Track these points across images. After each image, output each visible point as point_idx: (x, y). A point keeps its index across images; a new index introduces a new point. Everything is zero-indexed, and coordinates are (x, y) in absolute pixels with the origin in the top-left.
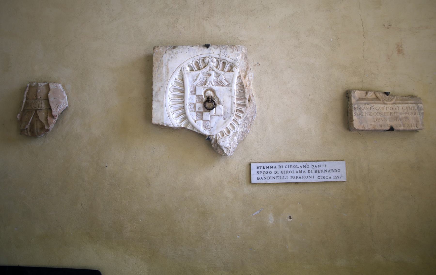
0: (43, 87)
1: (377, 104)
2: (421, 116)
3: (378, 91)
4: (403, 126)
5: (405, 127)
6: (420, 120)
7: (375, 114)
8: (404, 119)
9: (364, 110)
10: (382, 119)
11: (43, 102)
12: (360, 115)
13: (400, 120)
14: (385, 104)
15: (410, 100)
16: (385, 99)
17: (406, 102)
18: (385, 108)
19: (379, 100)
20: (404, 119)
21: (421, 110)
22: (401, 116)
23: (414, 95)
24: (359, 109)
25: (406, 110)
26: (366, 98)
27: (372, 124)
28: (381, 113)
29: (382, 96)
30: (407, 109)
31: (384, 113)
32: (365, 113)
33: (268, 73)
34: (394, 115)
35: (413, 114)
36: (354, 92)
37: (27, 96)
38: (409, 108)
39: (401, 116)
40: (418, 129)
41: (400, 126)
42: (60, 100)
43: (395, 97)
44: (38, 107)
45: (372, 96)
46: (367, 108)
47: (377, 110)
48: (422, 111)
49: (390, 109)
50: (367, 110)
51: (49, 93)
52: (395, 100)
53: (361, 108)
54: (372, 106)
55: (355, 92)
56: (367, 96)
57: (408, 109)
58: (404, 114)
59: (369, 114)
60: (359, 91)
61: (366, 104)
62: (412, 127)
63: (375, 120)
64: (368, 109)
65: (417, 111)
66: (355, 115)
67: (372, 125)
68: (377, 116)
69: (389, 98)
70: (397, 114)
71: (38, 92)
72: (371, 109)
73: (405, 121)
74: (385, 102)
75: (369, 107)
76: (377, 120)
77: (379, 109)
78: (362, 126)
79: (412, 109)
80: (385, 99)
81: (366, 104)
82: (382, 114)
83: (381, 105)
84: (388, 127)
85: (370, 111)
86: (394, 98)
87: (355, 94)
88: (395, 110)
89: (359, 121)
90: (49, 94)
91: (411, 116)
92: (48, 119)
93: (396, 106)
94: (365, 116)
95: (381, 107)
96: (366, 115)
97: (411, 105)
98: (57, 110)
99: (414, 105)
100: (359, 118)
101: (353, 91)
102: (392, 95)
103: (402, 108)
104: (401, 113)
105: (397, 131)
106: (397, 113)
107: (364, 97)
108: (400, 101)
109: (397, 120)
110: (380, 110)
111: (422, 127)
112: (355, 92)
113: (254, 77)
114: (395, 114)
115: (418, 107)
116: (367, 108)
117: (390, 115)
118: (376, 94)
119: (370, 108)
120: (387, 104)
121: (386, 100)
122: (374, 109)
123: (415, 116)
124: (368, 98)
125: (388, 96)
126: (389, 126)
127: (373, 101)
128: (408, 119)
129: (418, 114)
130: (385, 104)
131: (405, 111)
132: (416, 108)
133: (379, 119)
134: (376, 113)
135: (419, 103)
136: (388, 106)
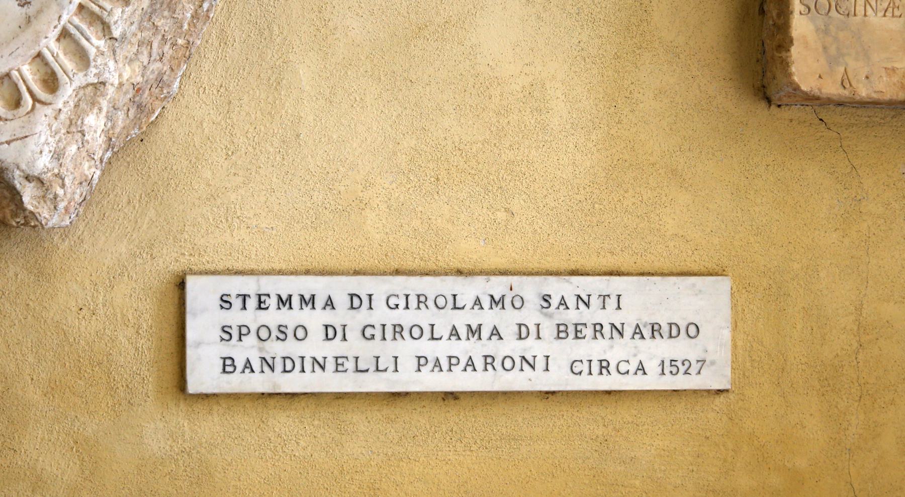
12: (833, 13)
27: (897, 65)
66: (803, 8)
67: (894, 70)
78: (839, 78)
89: (825, 48)
96: (870, 11)
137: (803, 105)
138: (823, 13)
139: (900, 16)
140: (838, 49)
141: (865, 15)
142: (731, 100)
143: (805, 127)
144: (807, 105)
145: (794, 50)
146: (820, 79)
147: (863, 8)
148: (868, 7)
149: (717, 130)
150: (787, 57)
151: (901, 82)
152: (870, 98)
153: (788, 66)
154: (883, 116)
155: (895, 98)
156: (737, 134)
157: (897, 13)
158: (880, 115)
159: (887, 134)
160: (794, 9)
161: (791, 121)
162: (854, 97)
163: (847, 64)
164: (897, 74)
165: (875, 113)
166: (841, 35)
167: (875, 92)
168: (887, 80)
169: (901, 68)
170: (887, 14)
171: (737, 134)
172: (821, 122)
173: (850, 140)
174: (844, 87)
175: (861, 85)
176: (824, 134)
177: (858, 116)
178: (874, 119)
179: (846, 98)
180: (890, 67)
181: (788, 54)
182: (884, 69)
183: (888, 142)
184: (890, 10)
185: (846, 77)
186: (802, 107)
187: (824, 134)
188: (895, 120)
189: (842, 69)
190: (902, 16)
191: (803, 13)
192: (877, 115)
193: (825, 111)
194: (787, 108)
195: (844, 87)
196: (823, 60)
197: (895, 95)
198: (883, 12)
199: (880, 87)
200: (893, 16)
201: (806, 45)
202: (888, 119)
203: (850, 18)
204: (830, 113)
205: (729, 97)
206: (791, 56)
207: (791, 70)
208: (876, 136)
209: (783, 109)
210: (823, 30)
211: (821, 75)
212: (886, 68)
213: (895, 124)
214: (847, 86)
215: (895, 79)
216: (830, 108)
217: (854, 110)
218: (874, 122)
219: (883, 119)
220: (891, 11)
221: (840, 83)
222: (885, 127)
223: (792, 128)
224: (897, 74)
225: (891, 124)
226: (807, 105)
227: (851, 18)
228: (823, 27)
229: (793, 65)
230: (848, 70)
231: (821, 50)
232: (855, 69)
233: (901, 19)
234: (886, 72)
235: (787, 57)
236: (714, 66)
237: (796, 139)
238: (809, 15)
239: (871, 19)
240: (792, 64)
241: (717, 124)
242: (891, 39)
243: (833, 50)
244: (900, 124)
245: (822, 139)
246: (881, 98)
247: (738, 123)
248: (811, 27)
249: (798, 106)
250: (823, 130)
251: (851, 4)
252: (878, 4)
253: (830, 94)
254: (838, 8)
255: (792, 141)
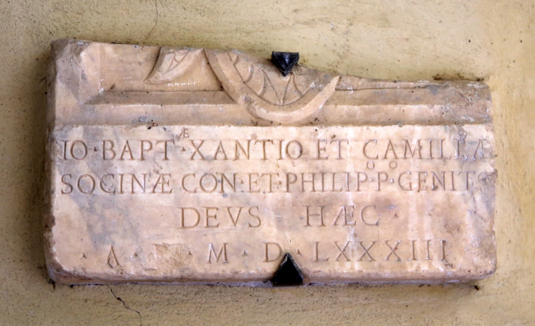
1: (206, 124)
2: (478, 197)
3: (227, 50)
4: (358, 255)
5: (373, 260)
6: (468, 220)
7: (192, 184)
8: (370, 212)
9: (127, 156)
10: (235, 216)
12: (98, 191)
13: (342, 221)
14: (257, 122)
15: (418, 101)
16: (260, 97)
17: (394, 109)
18: (257, 152)
19: (230, 99)
20: (370, 212)
21: (477, 159)
22: (349, 193)
23: (467, 76)
24: (91, 153)
25: (385, 158)
26: (148, 87)
27: (169, 242)
28: (230, 177)
29: (250, 77)
30: (390, 155)
31: (246, 179)
32: (128, 179)
33: (50, 12)
34: (308, 187)
35: (429, 183)
36: (77, 52)
38: (407, 145)
39: (351, 197)
40: (450, 272)
41: (344, 255)
43: (326, 82)
45: (188, 73)
46: (147, 146)
47: (203, 158)
48: (487, 167)
49: (284, 155)
50: (143, 159)
52: (327, 103)
53: (108, 145)
54: (178, 138)
55: (81, 50)
56: (161, 75)
57: (400, 153)
58: (375, 185)
59: (154, 181)
60: (109, 48)
61: (138, 122)
62: (414, 259)
63: (191, 219)
64: (150, 154)
65: (453, 165)
66: (64, 187)
67: (165, 246)
68: (203, 195)
69: (291, 85)
70: (328, 186)
72: (169, 156)
73: (377, 224)
74: (262, 112)
75: (158, 142)
76: (204, 217)
77: (220, 156)
78: (105, 256)
79: (425, 151)
80: (264, 92)
81: (138, 122)
82: (233, 187)
83: (233, 129)
84: (267, 260)
85: (163, 164)
86: (320, 90)
87: (80, 61)
88: (319, 158)
89: (90, 227)
91: (411, 193)
93: (323, 133)
94: (125, 195)
95: (233, 144)
96: (137, 188)
97: (418, 129)
99: (438, 131)
100: (91, 210)
101: (69, 47)
102: (314, 73)
103: (362, 144)
104: (354, 175)
105: (350, 285)
106: (328, 179)
107: (136, 85)
108: (356, 108)
109: (326, 221)
110: (226, 158)
111: (477, 260)
112: (78, 54)
114: (318, 185)
115: (461, 144)
116: (147, 146)
117: (285, 189)
118: (213, 65)
119: (162, 146)
120: (271, 123)
121: (269, 102)
122: (187, 155)
123: (439, 196)
124: (162, 88)
125: (284, 75)
126: (274, 252)
127: (188, 108)
128: (396, 215)
129: (459, 182)
130: (256, 124)
131: (382, 165)
132: (449, 148)
133: (212, 213)
134: (198, 177)
135: (472, 120)
136: (276, 133)
137: (97, 285)
138: (87, 191)
139: (171, 192)
140: (104, 226)
141: (133, 192)
142: (22, 282)
143: (101, 306)
144: (101, 285)
145: (55, 230)
146: (84, 259)
147: (130, 185)
148: (135, 183)
149: (7, 313)
150: (49, 237)
151: (174, 259)
152: (142, 276)
153: (50, 247)
154: (185, 293)
155: (169, 275)
156: (28, 317)
157: (167, 188)
158: (182, 292)
159: (190, 311)
160: (55, 188)
161: (86, 301)
162: (123, 275)
163: (113, 243)
164: (170, 251)
165: (177, 290)
166: (107, 213)
167: (146, 270)
168: (158, 258)
169: (173, 245)
170: (156, 190)
171: (28, 317)
172: (118, 301)
173: (150, 319)
174: (111, 267)
175: (129, 264)
176: (122, 313)
177: (159, 293)
178: (175, 296)
179: (115, 277)
180: (161, 244)
181: (50, 234)
182: (155, 247)
183: (192, 319)
184: (160, 186)
185: (113, 256)
186: (97, 287)
187: (122, 313)
188: (198, 296)
189: (108, 248)
190: (172, 192)
191: (64, 191)
192: (179, 291)
193: (122, 289)
194: (80, 288)
195: (111, 267)
196: (87, 240)
197: (169, 272)
198: (152, 188)
199: (152, 264)
200: (163, 192)
201: (69, 224)
202: (192, 295)
203: (116, 196)
204: (128, 292)
205: (20, 279)
206: (52, 236)
207: (52, 250)
208: (179, 314)
209: (76, 289)
210: (87, 209)
211: (85, 254)
212: (156, 245)
213: (199, 300)
214: (114, 264)
215: (168, 256)
216: (127, 286)
217: (154, 288)
218: (176, 299)
219: (186, 296)
220: (161, 187)
221: (106, 262)
222: (188, 305)
223: (87, 308)
224: (170, 251)
225: (194, 301)
226: (101, 285)
227: (118, 196)
228: (87, 205)
229: (54, 245)
230: (116, 248)
231: (85, 228)
232: (122, 247)
233: (171, 194)
234: (157, 249)
235: (49, 237)
236: (4, 247)
237: (92, 320)
238: (72, 194)
239: (139, 195)
240: (53, 244)
241: (7, 307)
242: (162, 215)
243: (98, 229)
244: (204, 300)
245: (121, 318)
246: (153, 276)
247: (30, 306)
248: (75, 206)
249: (92, 286)
250: (121, 309)
251: (117, 181)
252: (147, 180)
253: (96, 273)
254: (103, 186)
255: (88, 322)
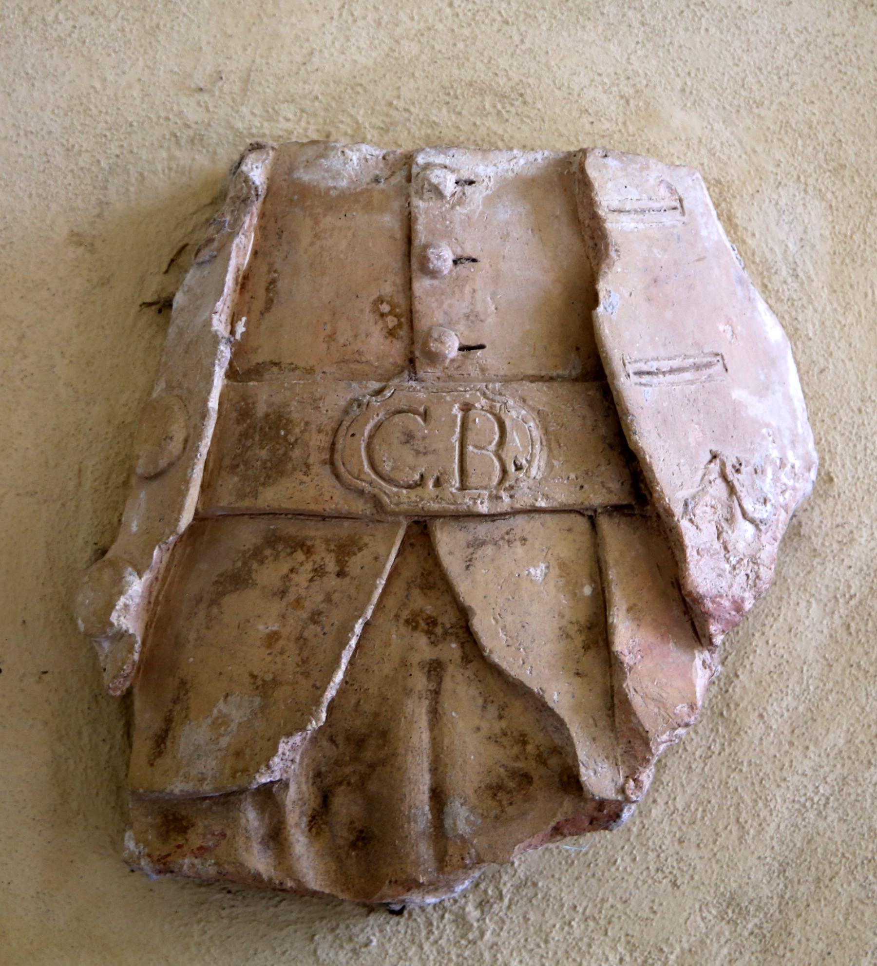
0: (491, 201)
11: (515, 413)
37: (240, 328)
42: (739, 394)
44: (463, 487)
51: (602, 287)
71: (434, 274)
90: (600, 309)
92: (628, 659)
98: (730, 536)
113: (178, 281)
